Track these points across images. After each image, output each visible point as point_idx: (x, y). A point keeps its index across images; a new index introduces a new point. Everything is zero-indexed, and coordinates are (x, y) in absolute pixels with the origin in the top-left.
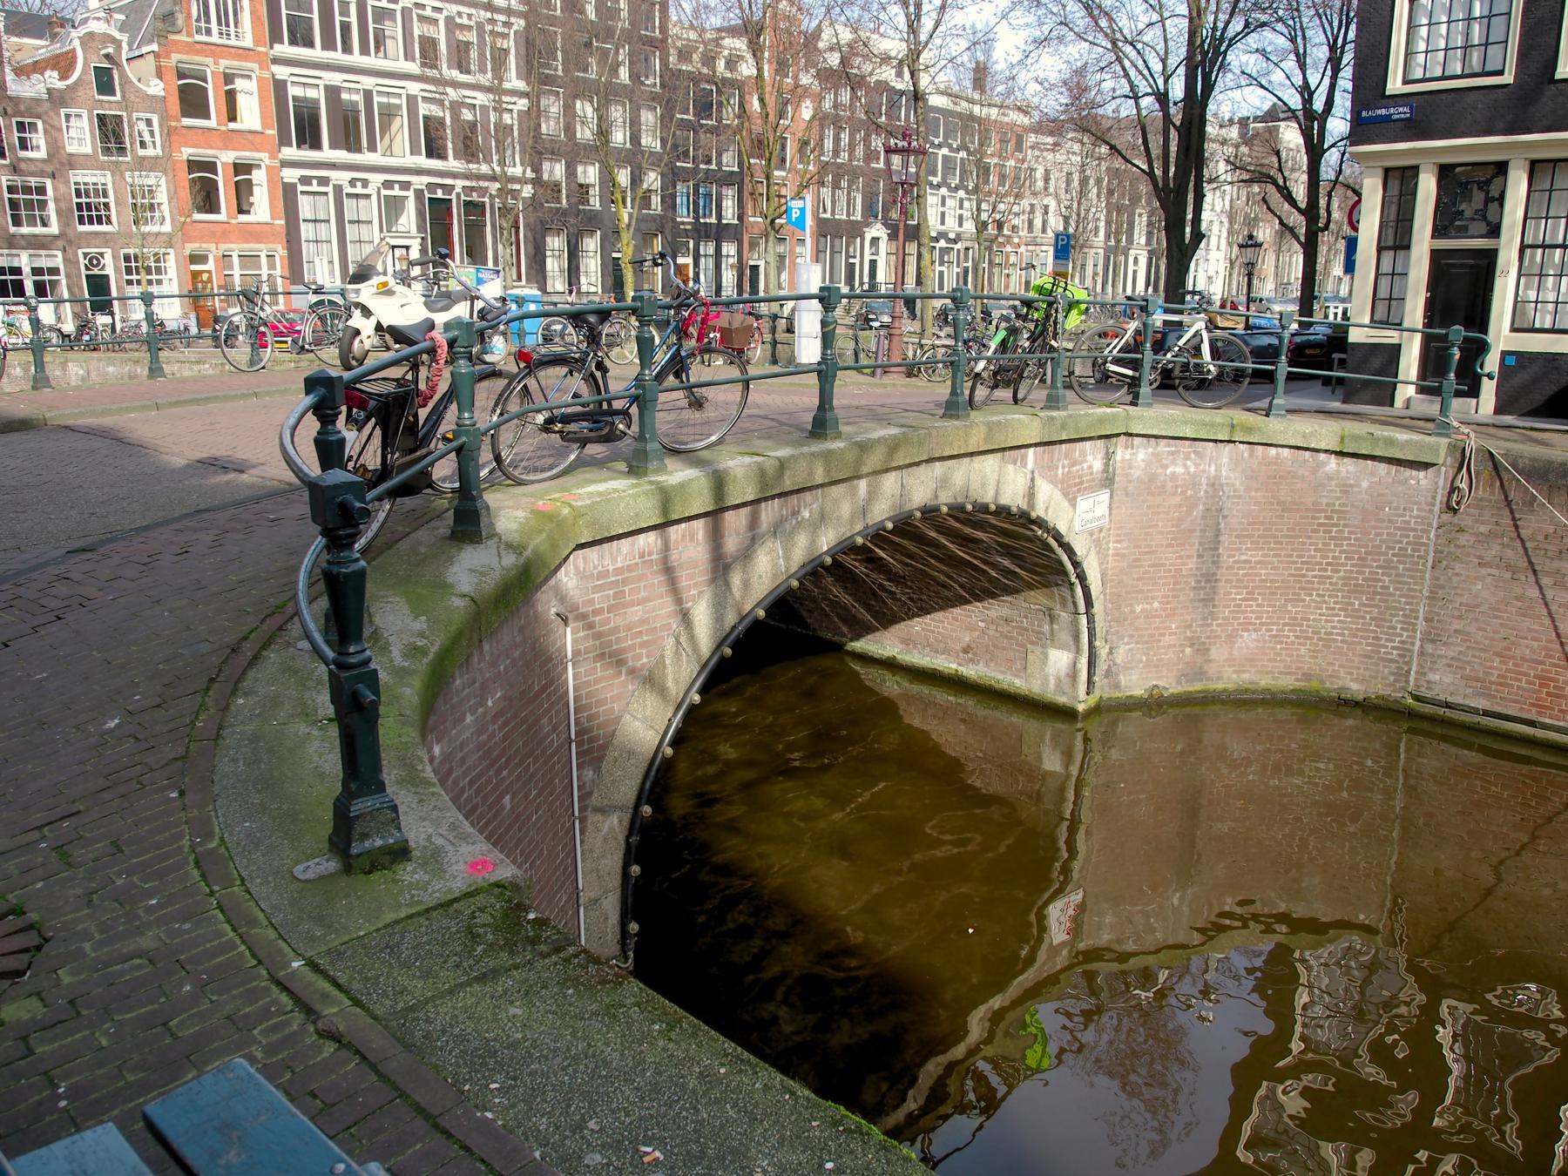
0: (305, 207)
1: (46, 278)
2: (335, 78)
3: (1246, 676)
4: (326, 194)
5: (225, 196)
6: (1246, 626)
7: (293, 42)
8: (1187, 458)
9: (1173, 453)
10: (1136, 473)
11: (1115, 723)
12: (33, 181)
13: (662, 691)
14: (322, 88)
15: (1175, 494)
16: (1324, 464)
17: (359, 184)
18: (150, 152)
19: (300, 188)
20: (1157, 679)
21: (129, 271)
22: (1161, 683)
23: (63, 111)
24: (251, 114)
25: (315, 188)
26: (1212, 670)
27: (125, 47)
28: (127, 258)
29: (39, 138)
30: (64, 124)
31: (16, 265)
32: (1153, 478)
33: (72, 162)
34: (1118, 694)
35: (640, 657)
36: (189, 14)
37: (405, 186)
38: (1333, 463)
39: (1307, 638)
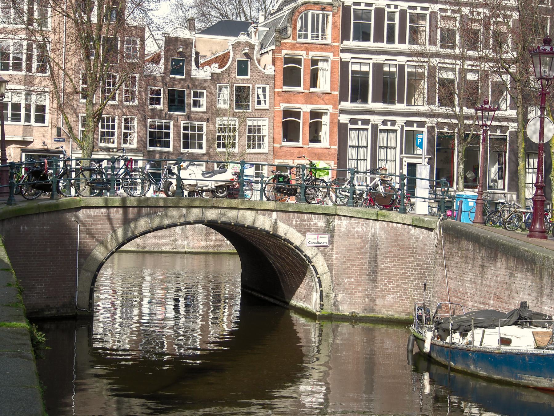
0: (382, 139)
2: (379, 59)
3: (390, 313)
4: (367, 130)
5: (304, 131)
7: (356, 39)
8: (363, 225)
9: (357, 223)
10: (343, 230)
11: (338, 326)
12: (196, 123)
13: (106, 247)
14: (371, 65)
15: (358, 238)
16: (411, 230)
17: (389, 124)
19: (350, 126)
20: (355, 309)
22: (356, 311)
23: (218, 85)
24: (325, 83)
25: (360, 126)
26: (377, 308)
27: (256, 48)
29: (204, 100)
33: (219, 113)
34: (339, 313)
36: (295, 28)
37: (421, 124)
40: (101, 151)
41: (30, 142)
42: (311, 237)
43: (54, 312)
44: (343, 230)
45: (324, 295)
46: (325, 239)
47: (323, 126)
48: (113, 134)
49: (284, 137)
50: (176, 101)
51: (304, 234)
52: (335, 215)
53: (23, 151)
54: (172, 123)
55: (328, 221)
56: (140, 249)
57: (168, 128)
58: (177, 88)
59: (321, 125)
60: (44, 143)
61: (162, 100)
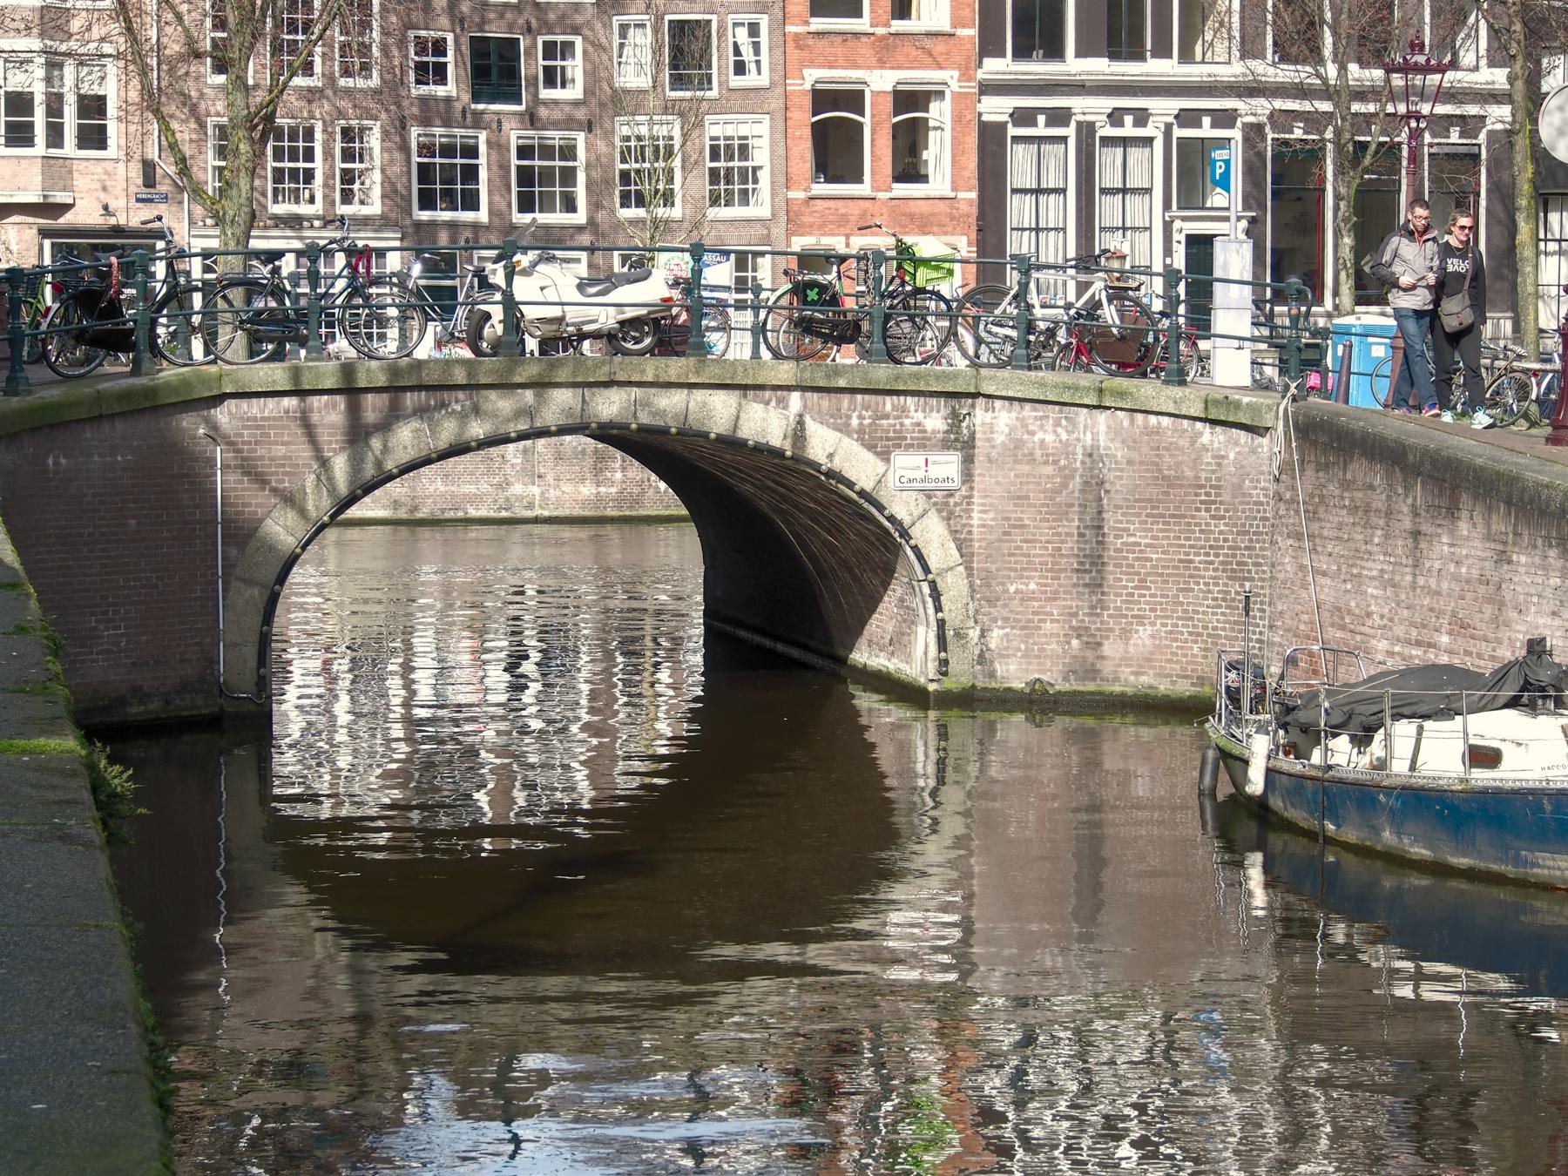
0: (1020, 166)
3: (1144, 679)
5: (876, 149)
6: (1140, 619)
8: (1057, 424)
9: (1041, 418)
12: (555, 137)
15: (1046, 463)
16: (1201, 434)
17: (1129, 119)
18: (750, 80)
19: (1012, 131)
22: (1045, 678)
25: (1041, 129)
26: (1107, 668)
29: (575, 67)
30: (616, 40)
32: (1019, 444)
33: (621, 102)
34: (994, 685)
35: (282, 481)
37: (1224, 119)
38: (1205, 429)
39: (1198, 634)
41: (66, 208)
42: (907, 464)
43: (155, 705)
46: (947, 466)
47: (931, 134)
48: (309, 176)
51: (885, 456)
53: (44, 233)
54: (483, 137)
56: (402, 514)
57: (472, 152)
59: (927, 129)
60: (106, 208)
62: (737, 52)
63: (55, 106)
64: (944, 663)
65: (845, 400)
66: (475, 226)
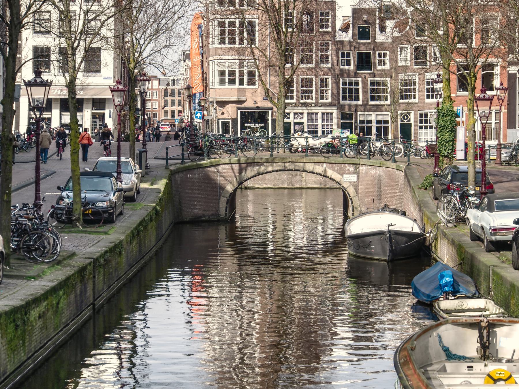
1: (382, 125)
21: (421, 122)
28: (421, 115)
29: (387, 59)
31: (369, 119)
40: (302, 106)
41: (244, 102)
42: (346, 177)
43: (207, 218)
44: (364, 172)
45: (354, 208)
46: (354, 178)
47: (494, 76)
48: (311, 92)
49: (460, 88)
50: (364, 61)
51: (342, 175)
52: (359, 164)
53: (238, 109)
54: (360, 79)
55: (355, 168)
56: (322, 186)
57: (357, 84)
58: (363, 50)
59: (493, 75)
60: (255, 102)
61: (352, 62)
62: (435, 54)
63: (241, 74)
64: (353, 214)
65: (334, 165)
66: (356, 105)
